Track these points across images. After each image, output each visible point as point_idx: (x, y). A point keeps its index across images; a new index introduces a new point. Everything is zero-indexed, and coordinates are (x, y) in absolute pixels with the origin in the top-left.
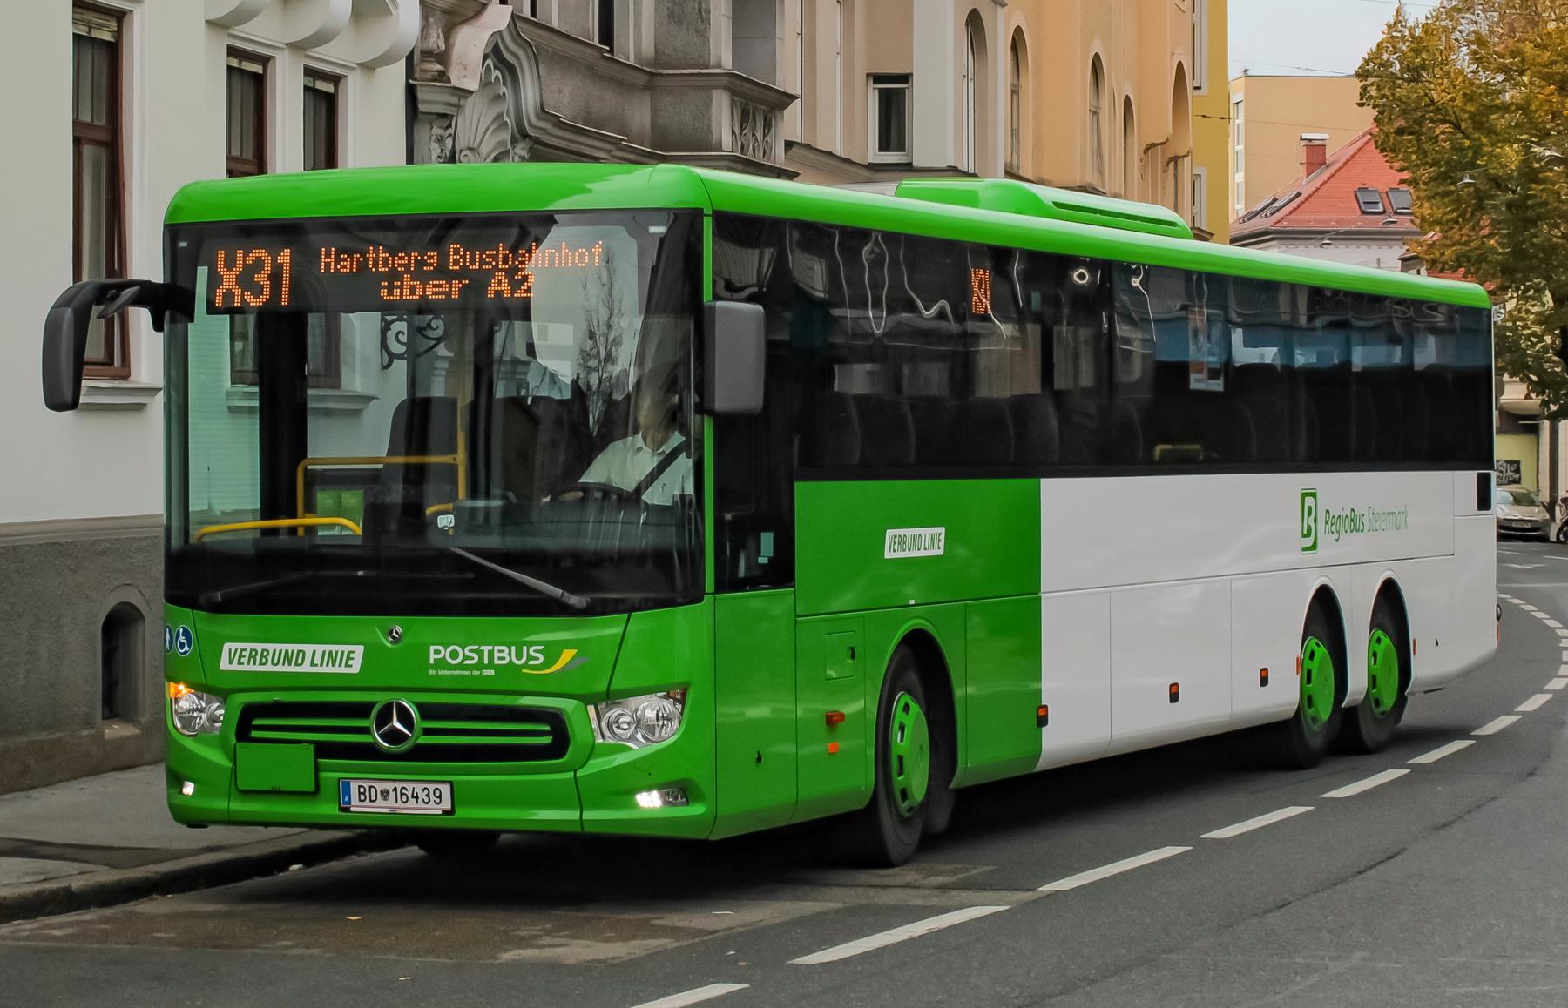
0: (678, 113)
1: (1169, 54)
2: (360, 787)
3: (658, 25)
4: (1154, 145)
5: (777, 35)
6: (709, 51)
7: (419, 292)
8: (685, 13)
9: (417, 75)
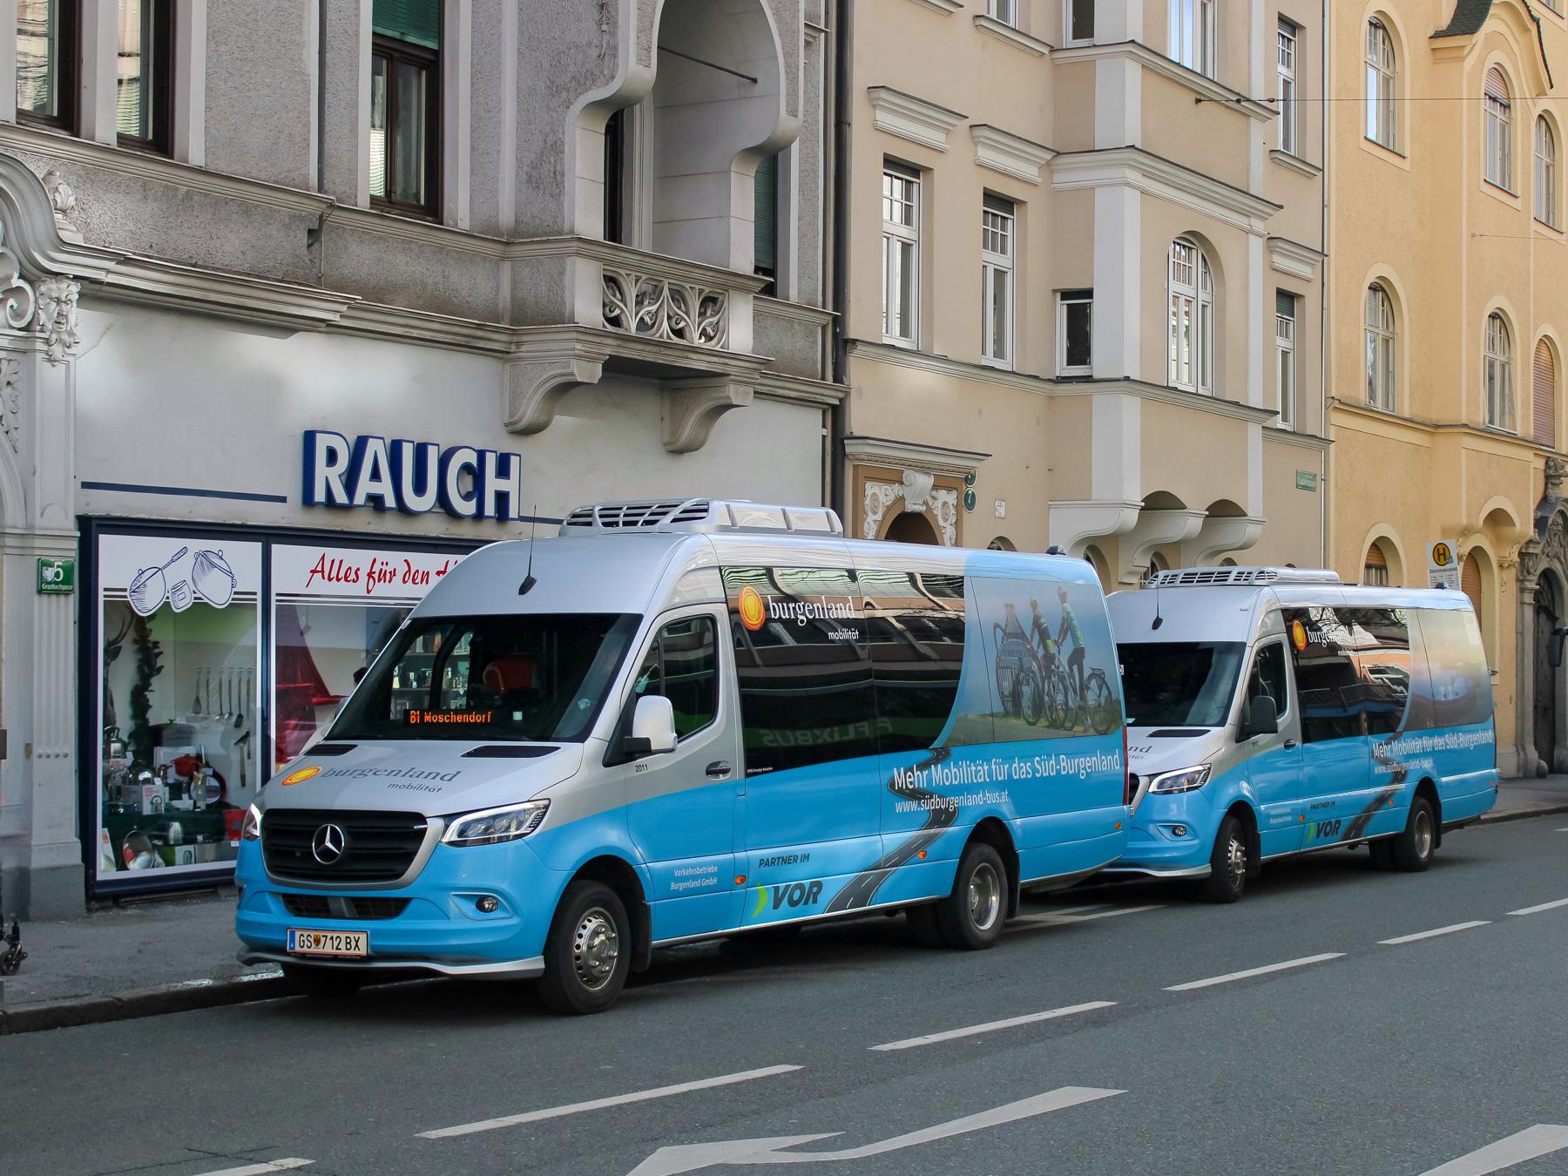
2: (347, 937)
3: (519, 191)
5: (733, 212)
6: (564, 217)
8: (542, 177)
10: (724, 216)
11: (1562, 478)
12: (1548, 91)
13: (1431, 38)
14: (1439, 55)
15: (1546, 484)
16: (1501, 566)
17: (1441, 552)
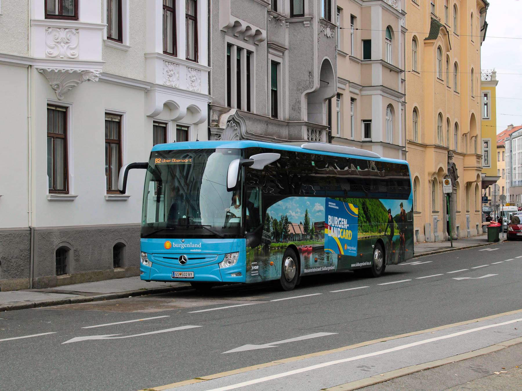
0: (294, 131)
1: (469, 111)
3: (290, 111)
4: (473, 137)
9: (211, 125)
10: (321, 113)
11: (452, 157)
12: (450, 51)
13: (424, 40)
14: (426, 44)
15: (448, 159)
16: (440, 182)
17: (447, 182)
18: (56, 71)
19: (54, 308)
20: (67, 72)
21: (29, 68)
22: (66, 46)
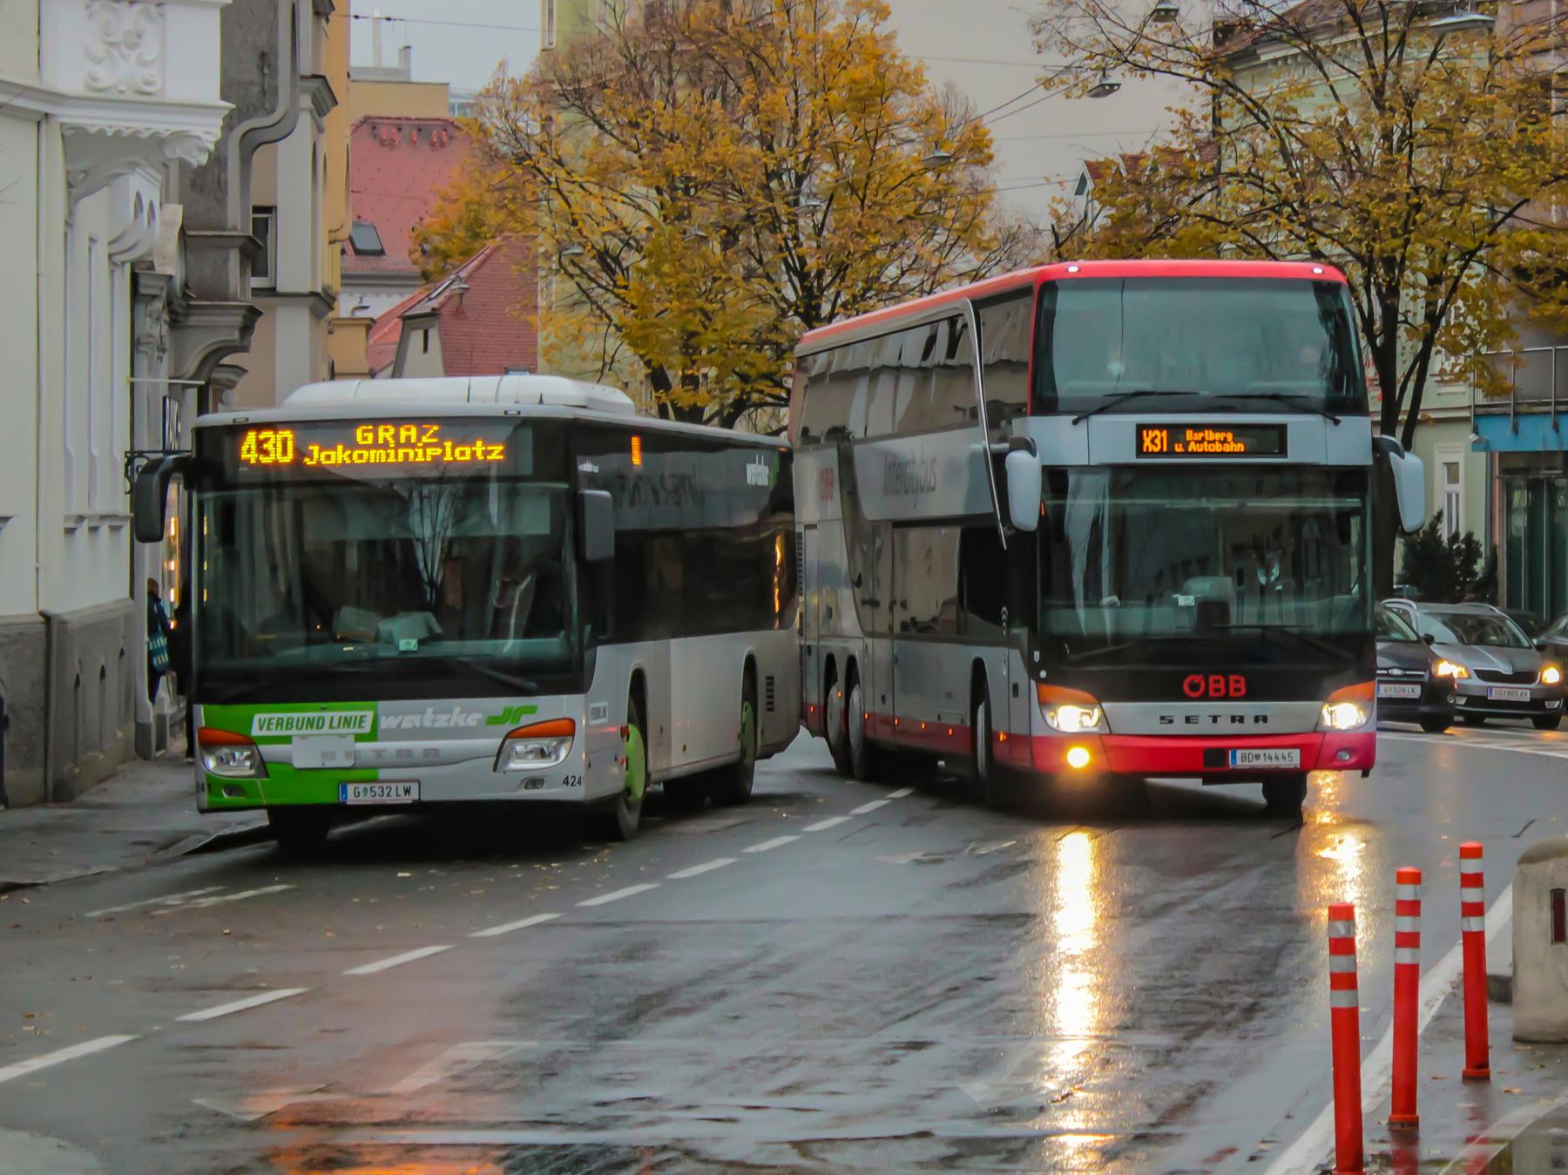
7: (365, 457)
18: (110, 133)
19: (1166, 891)
20: (135, 136)
21: (44, 126)
22: (134, 55)
